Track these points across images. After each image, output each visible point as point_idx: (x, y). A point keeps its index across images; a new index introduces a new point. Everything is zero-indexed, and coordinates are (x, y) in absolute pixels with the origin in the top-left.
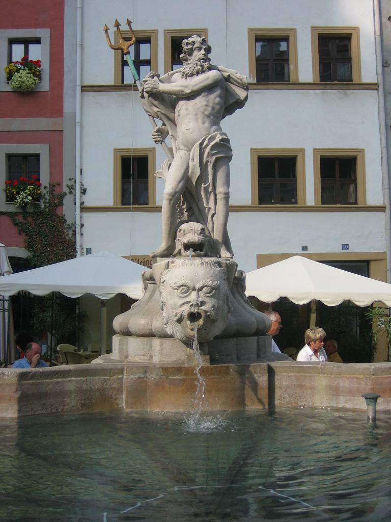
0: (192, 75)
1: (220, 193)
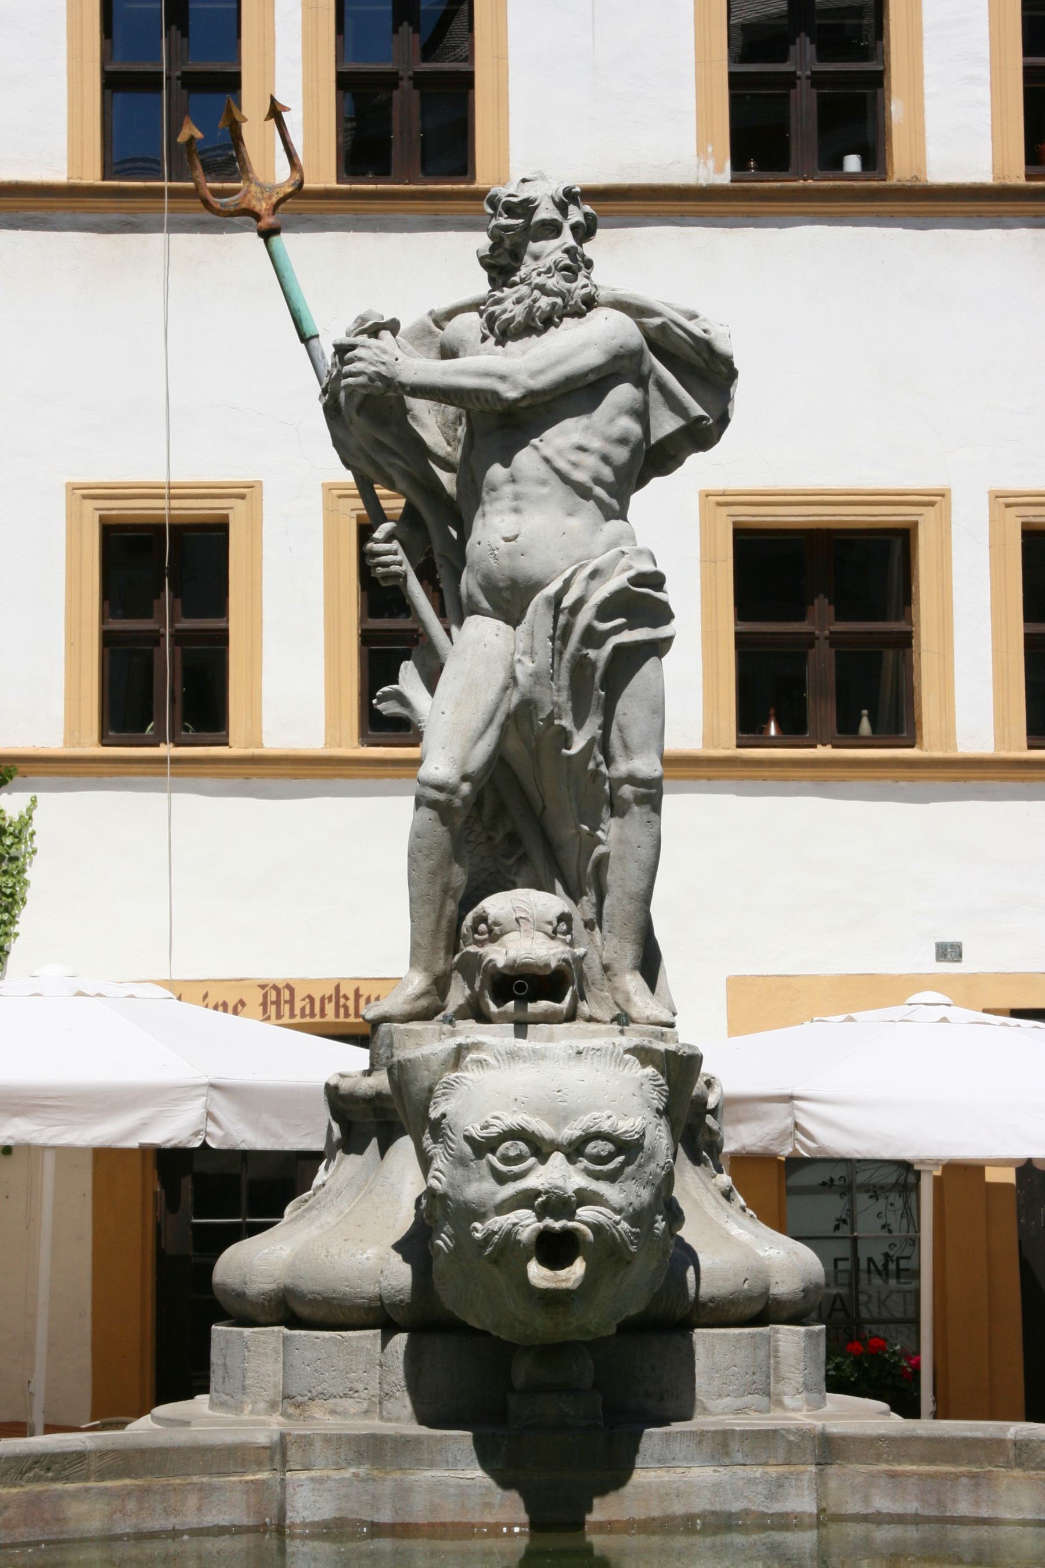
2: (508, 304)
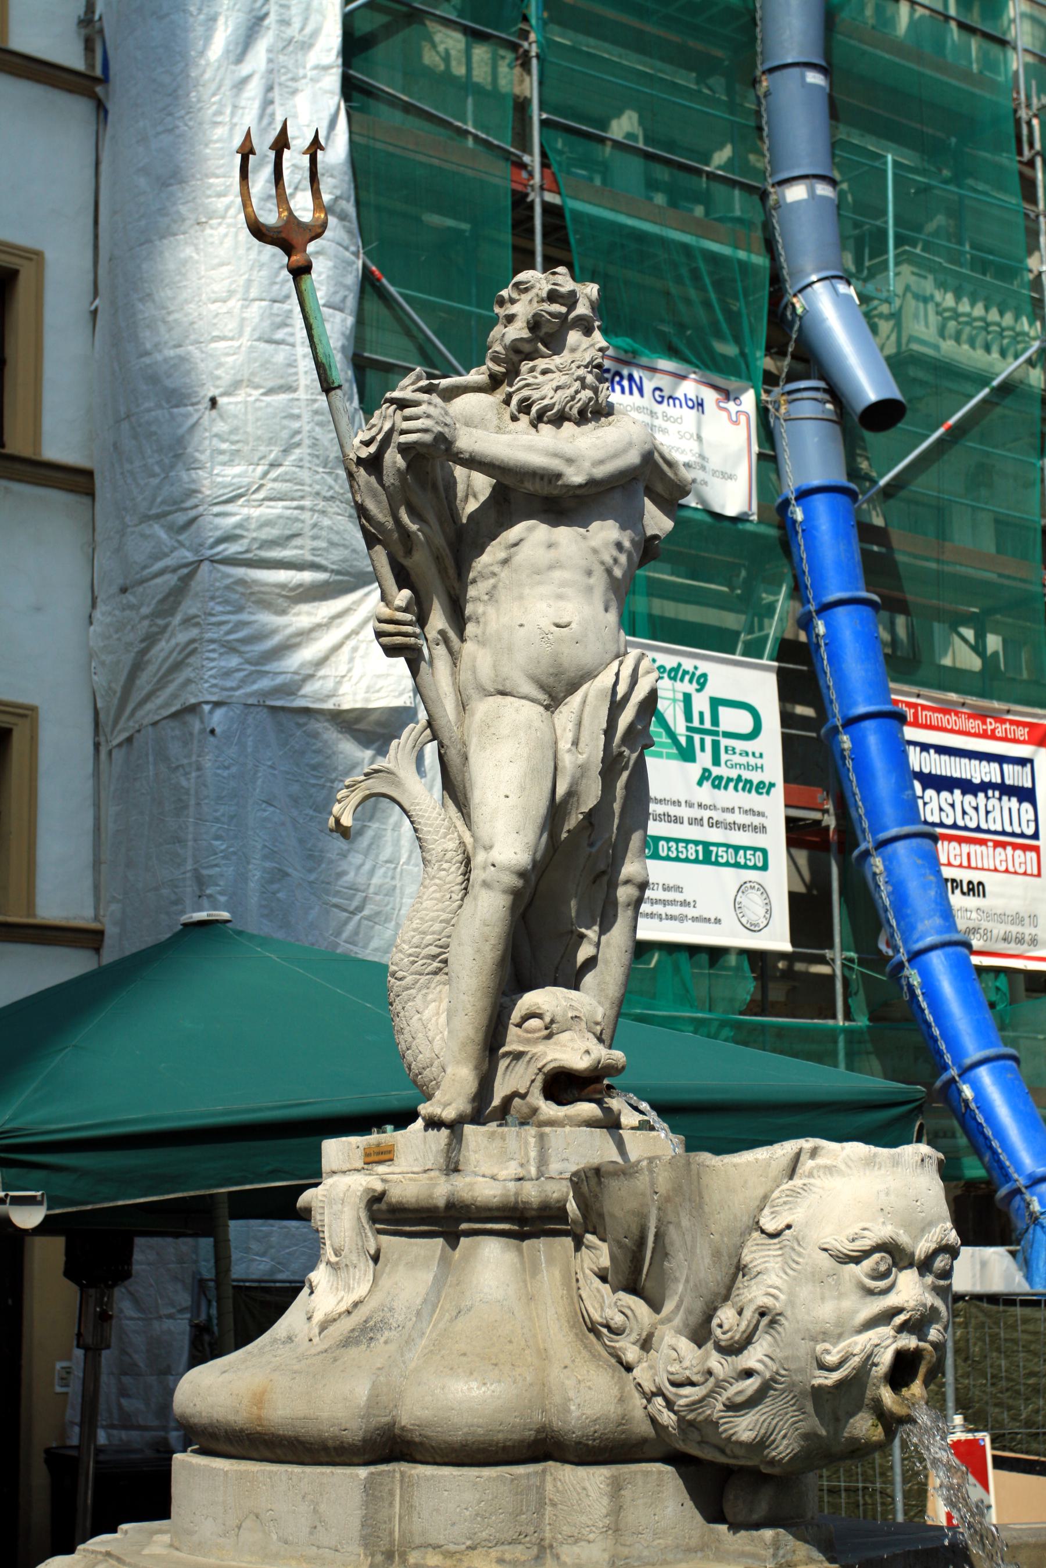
0: (560, 419)
1: (627, 882)
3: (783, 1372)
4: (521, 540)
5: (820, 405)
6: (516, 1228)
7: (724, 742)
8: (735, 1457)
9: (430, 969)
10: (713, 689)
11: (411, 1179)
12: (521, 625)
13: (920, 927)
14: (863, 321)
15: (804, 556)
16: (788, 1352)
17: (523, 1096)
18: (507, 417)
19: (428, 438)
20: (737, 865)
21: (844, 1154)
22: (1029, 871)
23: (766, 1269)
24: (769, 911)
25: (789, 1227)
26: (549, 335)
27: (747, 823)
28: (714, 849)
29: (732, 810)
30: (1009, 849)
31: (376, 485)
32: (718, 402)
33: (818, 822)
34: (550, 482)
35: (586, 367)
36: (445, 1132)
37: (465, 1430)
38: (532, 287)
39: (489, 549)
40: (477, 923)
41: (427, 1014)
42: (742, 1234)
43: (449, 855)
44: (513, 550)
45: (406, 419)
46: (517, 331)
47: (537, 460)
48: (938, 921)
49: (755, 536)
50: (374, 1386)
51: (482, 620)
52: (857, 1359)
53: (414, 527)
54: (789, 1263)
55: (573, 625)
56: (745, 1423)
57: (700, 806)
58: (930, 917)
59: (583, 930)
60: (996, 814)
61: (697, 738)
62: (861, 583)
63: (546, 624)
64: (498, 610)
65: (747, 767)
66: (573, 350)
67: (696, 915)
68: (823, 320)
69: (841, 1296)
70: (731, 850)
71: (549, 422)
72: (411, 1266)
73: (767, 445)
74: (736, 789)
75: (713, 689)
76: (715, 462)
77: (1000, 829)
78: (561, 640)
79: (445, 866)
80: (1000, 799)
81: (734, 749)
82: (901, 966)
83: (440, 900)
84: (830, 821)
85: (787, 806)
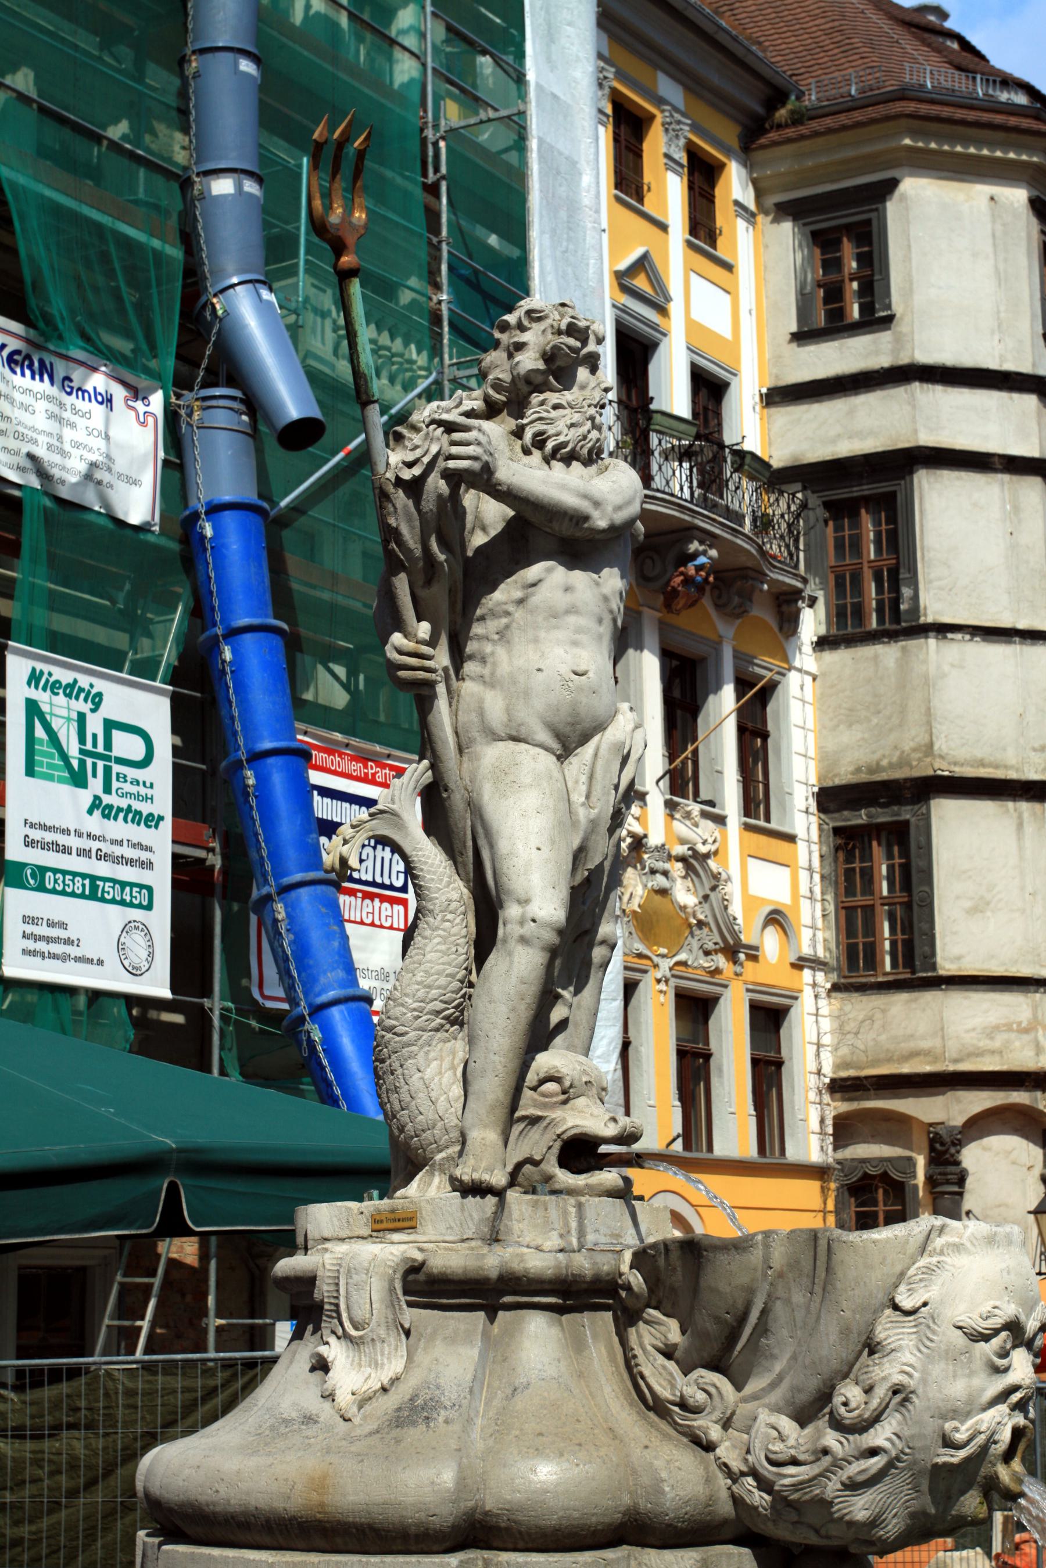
0: (569, 459)
2: (561, 425)
3: (907, 1450)
4: (540, 581)
5: (236, 416)
6: (561, 1301)
7: (116, 768)
8: (828, 1537)
9: (433, 1025)
10: (108, 710)
11: (446, 1249)
12: (539, 670)
13: (323, 980)
14: (286, 334)
15: (212, 575)
16: (914, 1431)
17: (536, 1163)
18: (518, 449)
19: (476, 466)
20: (122, 903)
21: (969, 1232)
22: (395, 926)
23: (901, 1346)
24: (151, 954)
25: (925, 1304)
26: (560, 369)
27: (135, 857)
28: (100, 883)
29: (120, 843)
30: (377, 901)
31: (413, 510)
32: (126, 400)
33: (203, 861)
34: (577, 524)
35: (596, 407)
36: (491, 1200)
37: (561, 1514)
38: (546, 317)
39: (502, 586)
40: (514, 980)
41: (429, 1073)
42: (875, 1312)
43: (454, 905)
44: (530, 590)
45: (454, 443)
46: (529, 361)
47: (570, 500)
48: (341, 974)
49: (156, 548)
50: (461, 1469)
51: (490, 660)
52: (983, 1437)
53: (442, 557)
54: (924, 1341)
55: (591, 674)
56: (861, 1503)
57: (89, 836)
58: (334, 969)
59: (560, 990)
60: (369, 863)
61: (89, 761)
62: (270, 610)
63: (565, 670)
64: (509, 651)
65: (138, 797)
66: (583, 387)
67: (78, 955)
68: (245, 326)
69: (971, 1374)
70: (117, 886)
71: (561, 460)
72: (452, 1340)
73: (172, 452)
74: (125, 820)
75: (108, 710)
76: (121, 465)
77: (370, 879)
78: (580, 689)
79: (450, 916)
80: (374, 848)
81: (125, 776)
82: (301, 1019)
83: (445, 953)
84: (216, 861)
85: (174, 842)
